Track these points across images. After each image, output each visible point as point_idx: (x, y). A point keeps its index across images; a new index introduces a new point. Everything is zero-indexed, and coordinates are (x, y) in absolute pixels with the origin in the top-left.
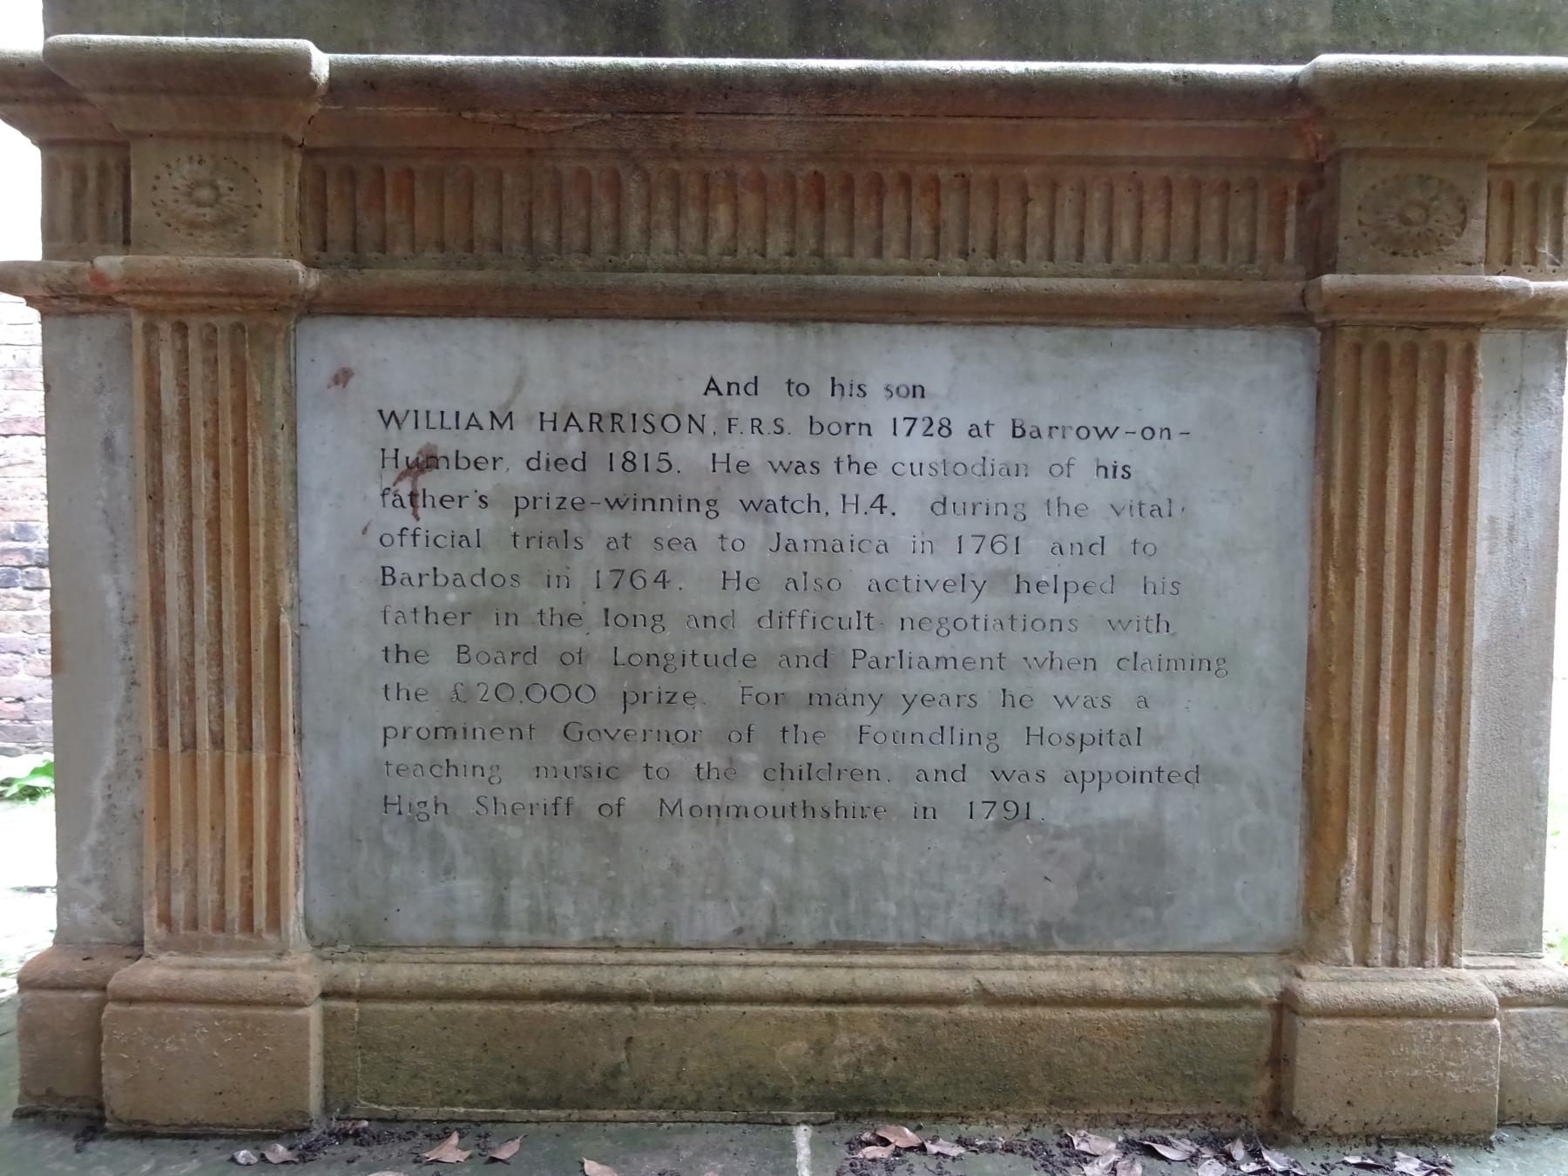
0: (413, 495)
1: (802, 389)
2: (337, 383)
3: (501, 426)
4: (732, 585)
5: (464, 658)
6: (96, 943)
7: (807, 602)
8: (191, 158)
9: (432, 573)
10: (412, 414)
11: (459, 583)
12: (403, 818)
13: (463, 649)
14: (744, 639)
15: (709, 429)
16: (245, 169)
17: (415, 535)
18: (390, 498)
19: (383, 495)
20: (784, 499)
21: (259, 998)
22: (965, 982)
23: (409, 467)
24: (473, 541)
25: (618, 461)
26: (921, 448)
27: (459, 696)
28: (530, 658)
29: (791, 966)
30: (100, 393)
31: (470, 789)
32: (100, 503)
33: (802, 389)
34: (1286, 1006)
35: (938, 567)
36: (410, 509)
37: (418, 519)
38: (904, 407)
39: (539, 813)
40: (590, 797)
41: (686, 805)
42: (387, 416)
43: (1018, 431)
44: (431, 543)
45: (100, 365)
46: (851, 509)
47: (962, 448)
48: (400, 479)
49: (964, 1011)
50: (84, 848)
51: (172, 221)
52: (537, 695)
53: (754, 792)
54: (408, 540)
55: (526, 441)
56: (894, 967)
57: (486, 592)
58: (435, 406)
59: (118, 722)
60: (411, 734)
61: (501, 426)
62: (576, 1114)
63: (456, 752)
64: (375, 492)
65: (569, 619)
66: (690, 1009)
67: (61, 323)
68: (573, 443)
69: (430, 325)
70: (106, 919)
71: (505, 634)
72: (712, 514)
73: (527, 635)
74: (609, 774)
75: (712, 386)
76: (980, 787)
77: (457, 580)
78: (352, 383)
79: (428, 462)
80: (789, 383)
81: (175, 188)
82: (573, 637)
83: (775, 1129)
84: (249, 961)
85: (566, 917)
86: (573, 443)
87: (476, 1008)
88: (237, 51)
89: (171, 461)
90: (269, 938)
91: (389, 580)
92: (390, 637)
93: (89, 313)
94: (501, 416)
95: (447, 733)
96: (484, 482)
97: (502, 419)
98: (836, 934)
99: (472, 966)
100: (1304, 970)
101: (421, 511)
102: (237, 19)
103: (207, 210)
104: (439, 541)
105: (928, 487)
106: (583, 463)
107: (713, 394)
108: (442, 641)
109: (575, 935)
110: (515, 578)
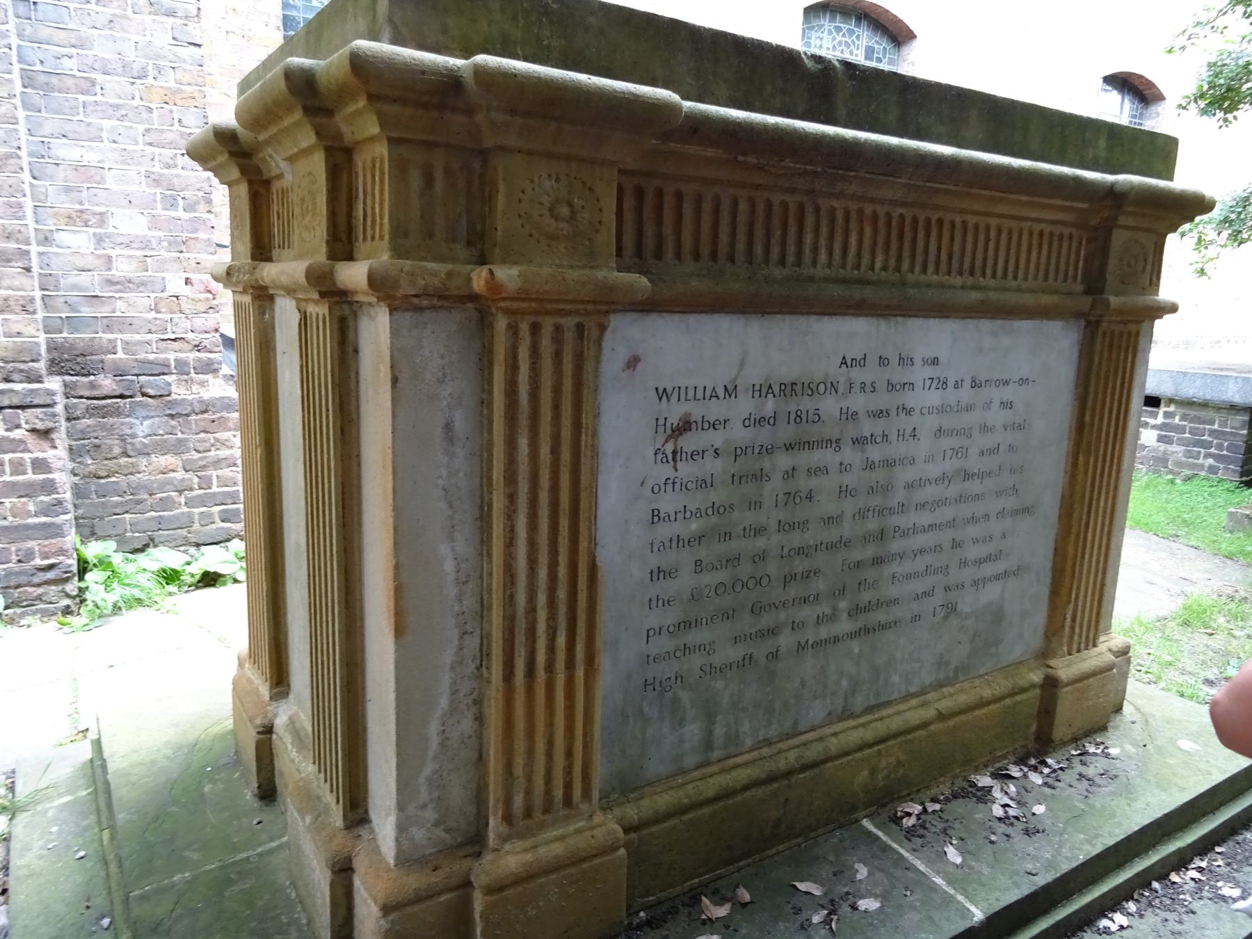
0: (674, 453)
1: (886, 362)
2: (629, 367)
3: (730, 396)
4: (843, 495)
5: (699, 569)
6: (431, 854)
7: (876, 501)
8: (550, 176)
9: (683, 510)
10: (677, 390)
11: (698, 515)
12: (656, 692)
13: (699, 563)
14: (848, 529)
15: (840, 392)
16: (590, 189)
17: (674, 483)
18: (660, 456)
19: (656, 454)
20: (872, 436)
21: (594, 852)
22: (930, 713)
23: (673, 431)
24: (709, 482)
25: (793, 416)
26: (933, 398)
27: (695, 597)
28: (736, 563)
29: (856, 727)
30: (443, 381)
31: (697, 660)
32: (440, 482)
33: (886, 362)
34: (1051, 684)
35: (934, 470)
36: (672, 463)
37: (676, 470)
38: (929, 372)
39: (734, 668)
40: (761, 650)
41: (810, 643)
42: (661, 392)
43: (975, 384)
44: (684, 488)
45: (442, 357)
46: (901, 438)
47: (951, 396)
48: (666, 441)
49: (932, 727)
50: (421, 780)
51: (534, 232)
52: (738, 588)
53: (845, 626)
54: (669, 487)
55: (745, 405)
56: (898, 713)
57: (714, 519)
58: (691, 383)
59: (452, 668)
60: (664, 631)
61: (730, 396)
62: (758, 857)
63: (692, 637)
64: (651, 452)
65: (760, 531)
66: (816, 770)
67: (407, 318)
68: (770, 405)
69: (692, 319)
70: (440, 832)
71: (722, 548)
72: (837, 449)
73: (736, 545)
74: (773, 632)
75: (844, 362)
76: (939, 598)
77: (698, 514)
78: (640, 366)
79: (685, 426)
80: (880, 358)
81: (542, 204)
82: (761, 543)
83: (853, 826)
84: (571, 828)
85: (745, 733)
86: (770, 405)
87: (706, 810)
88: (632, 97)
89: (523, 443)
90: (584, 807)
91: (656, 519)
92: (654, 561)
93: (433, 308)
94: (730, 388)
95: (686, 625)
96: (716, 438)
97: (730, 391)
98: (873, 702)
99: (697, 783)
100: (1052, 663)
101: (679, 465)
102: (563, 42)
103: (562, 225)
104: (688, 486)
105: (932, 421)
106: (773, 420)
107: (844, 366)
108: (685, 558)
109: (749, 742)
110: (731, 506)
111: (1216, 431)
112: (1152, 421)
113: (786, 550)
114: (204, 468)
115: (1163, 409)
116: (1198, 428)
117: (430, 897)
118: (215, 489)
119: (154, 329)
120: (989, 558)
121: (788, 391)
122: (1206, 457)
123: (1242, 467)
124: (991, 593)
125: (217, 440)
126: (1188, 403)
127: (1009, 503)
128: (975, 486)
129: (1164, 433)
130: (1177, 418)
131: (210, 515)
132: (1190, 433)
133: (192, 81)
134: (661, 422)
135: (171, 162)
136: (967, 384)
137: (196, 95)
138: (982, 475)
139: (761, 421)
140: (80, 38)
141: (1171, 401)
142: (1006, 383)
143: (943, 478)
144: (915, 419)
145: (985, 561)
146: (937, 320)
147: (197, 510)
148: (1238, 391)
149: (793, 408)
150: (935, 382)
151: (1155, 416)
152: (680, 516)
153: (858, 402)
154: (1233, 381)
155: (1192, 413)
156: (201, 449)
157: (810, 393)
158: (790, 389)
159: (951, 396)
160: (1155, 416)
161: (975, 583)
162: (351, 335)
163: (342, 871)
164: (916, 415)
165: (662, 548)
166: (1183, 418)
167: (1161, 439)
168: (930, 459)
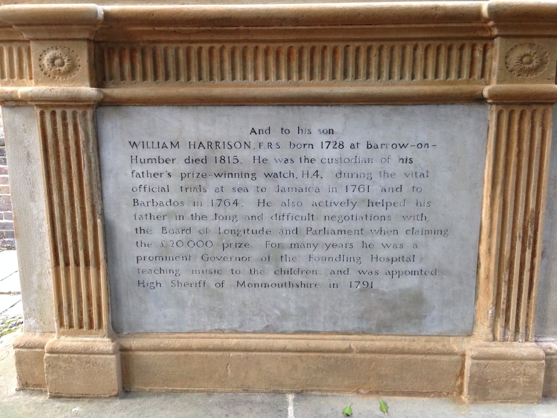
1: (287, 132)
25: (218, 159)
26: (333, 153)
33: (287, 132)
35: (338, 197)
40: (211, 280)
42: (132, 143)
43: (369, 146)
44: (151, 190)
47: (348, 152)
54: (142, 189)
71: (179, 223)
75: (253, 131)
78: (429, 171)
80: (282, 129)
94: (175, 144)
105: (335, 168)
106: (205, 160)
117: (31, 348)
134: (134, 157)
136: (363, 146)
144: (317, 166)
146: (289, 108)
153: (264, 153)
157: (230, 147)
158: (214, 145)
161: (391, 274)
165: (141, 218)
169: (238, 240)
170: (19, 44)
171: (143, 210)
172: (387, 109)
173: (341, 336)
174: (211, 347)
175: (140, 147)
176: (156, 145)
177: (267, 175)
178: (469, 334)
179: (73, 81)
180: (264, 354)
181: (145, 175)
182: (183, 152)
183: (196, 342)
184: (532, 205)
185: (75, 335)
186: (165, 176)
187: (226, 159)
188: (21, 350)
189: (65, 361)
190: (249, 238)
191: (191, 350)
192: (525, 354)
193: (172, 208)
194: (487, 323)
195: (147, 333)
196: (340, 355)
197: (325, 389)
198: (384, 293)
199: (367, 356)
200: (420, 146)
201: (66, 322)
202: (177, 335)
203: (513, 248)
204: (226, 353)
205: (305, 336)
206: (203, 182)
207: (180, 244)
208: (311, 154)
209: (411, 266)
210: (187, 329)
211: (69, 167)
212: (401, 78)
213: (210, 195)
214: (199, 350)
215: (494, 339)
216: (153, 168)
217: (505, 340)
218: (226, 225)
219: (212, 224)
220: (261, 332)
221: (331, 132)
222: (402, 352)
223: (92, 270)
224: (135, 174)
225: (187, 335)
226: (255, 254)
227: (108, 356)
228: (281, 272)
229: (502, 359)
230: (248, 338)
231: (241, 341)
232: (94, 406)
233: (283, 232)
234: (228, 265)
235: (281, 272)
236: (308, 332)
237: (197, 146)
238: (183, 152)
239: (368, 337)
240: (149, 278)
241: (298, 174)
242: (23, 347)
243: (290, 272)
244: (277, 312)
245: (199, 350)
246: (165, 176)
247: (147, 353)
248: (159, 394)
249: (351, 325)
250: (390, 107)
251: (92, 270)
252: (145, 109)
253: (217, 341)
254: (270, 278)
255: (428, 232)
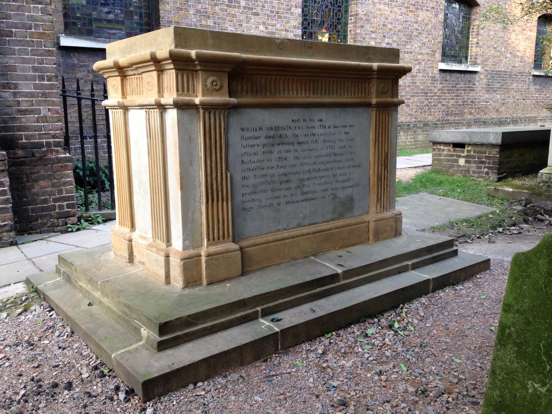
25: (279, 136)
26: (322, 131)
35: (324, 152)
38: (320, 123)
40: (275, 202)
54: (246, 154)
67: (180, 111)
75: (293, 121)
94: (261, 128)
105: (322, 138)
106: (273, 137)
111: (487, 156)
112: (463, 155)
113: (280, 174)
114: (59, 186)
115: (466, 149)
116: (481, 156)
117: (192, 258)
118: (64, 195)
119: (36, 129)
120: (346, 181)
121: (277, 128)
122: (484, 168)
123: (498, 171)
124: (348, 191)
125: (64, 174)
126: (475, 145)
127: (351, 163)
128: (338, 158)
129: (467, 159)
130: (472, 152)
131: (63, 206)
132: (478, 158)
133: (49, 29)
134: (243, 137)
135: (42, 62)
136: (332, 127)
137: (50, 34)
138: (341, 155)
139: (270, 137)
140: (7, 15)
141: (469, 145)
142: (346, 126)
143: (328, 155)
144: (316, 137)
145: (345, 181)
147: (57, 204)
148: (494, 139)
149: (279, 134)
150: (322, 126)
151: (463, 152)
152: (249, 162)
153: (297, 132)
154: (492, 134)
155: (478, 149)
156: (58, 178)
158: (277, 128)
159: (327, 130)
160: (463, 152)
161: (342, 188)
162: (164, 117)
163: (167, 257)
164: (316, 136)
166: (474, 152)
167: (466, 162)
168: (322, 149)
169: (287, 178)
170: (188, 72)
171: (246, 166)
172: (340, 109)
173: (326, 223)
174: (278, 239)
175: (245, 131)
176: (252, 129)
177: (298, 143)
178: (367, 213)
179: (221, 94)
180: (300, 238)
181: (247, 146)
182: (264, 133)
183: (270, 238)
184: (386, 151)
185: (215, 244)
186: (256, 146)
187: (282, 136)
188: (186, 260)
189: (216, 259)
190: (291, 177)
191: (270, 242)
192: (389, 216)
193: (259, 164)
194: (375, 206)
195: (246, 238)
196: (328, 232)
197: (324, 250)
198: (340, 199)
199: (338, 230)
200: (351, 126)
201: (211, 238)
202: (260, 237)
203: (382, 170)
204: (284, 241)
205: (313, 226)
206: (272, 149)
207: (262, 184)
208: (315, 131)
209: (349, 184)
210: (265, 232)
211: (156, 154)
212: (348, 95)
213: (275, 156)
214: (273, 241)
215: (377, 213)
216: (251, 142)
217: (381, 212)
218: (282, 171)
219: (275, 171)
220: (296, 228)
221: (321, 120)
222: (349, 225)
223: (225, 203)
224: (243, 146)
225: (265, 236)
226: (293, 185)
227: (236, 252)
228: (303, 193)
229: (383, 220)
230: (291, 232)
231: (289, 233)
232: (234, 282)
233: (305, 172)
234: (283, 193)
235: (303, 193)
236: (314, 224)
237: (270, 129)
238: (264, 133)
239: (336, 221)
240: (248, 205)
241: (310, 142)
242: (188, 258)
243: (306, 193)
244: (302, 215)
245: (273, 241)
246: (256, 146)
247: (250, 249)
248: (257, 270)
249: (329, 217)
250: (341, 108)
251: (225, 203)
252: (248, 110)
253: (279, 236)
254: (300, 197)
255: (354, 166)
